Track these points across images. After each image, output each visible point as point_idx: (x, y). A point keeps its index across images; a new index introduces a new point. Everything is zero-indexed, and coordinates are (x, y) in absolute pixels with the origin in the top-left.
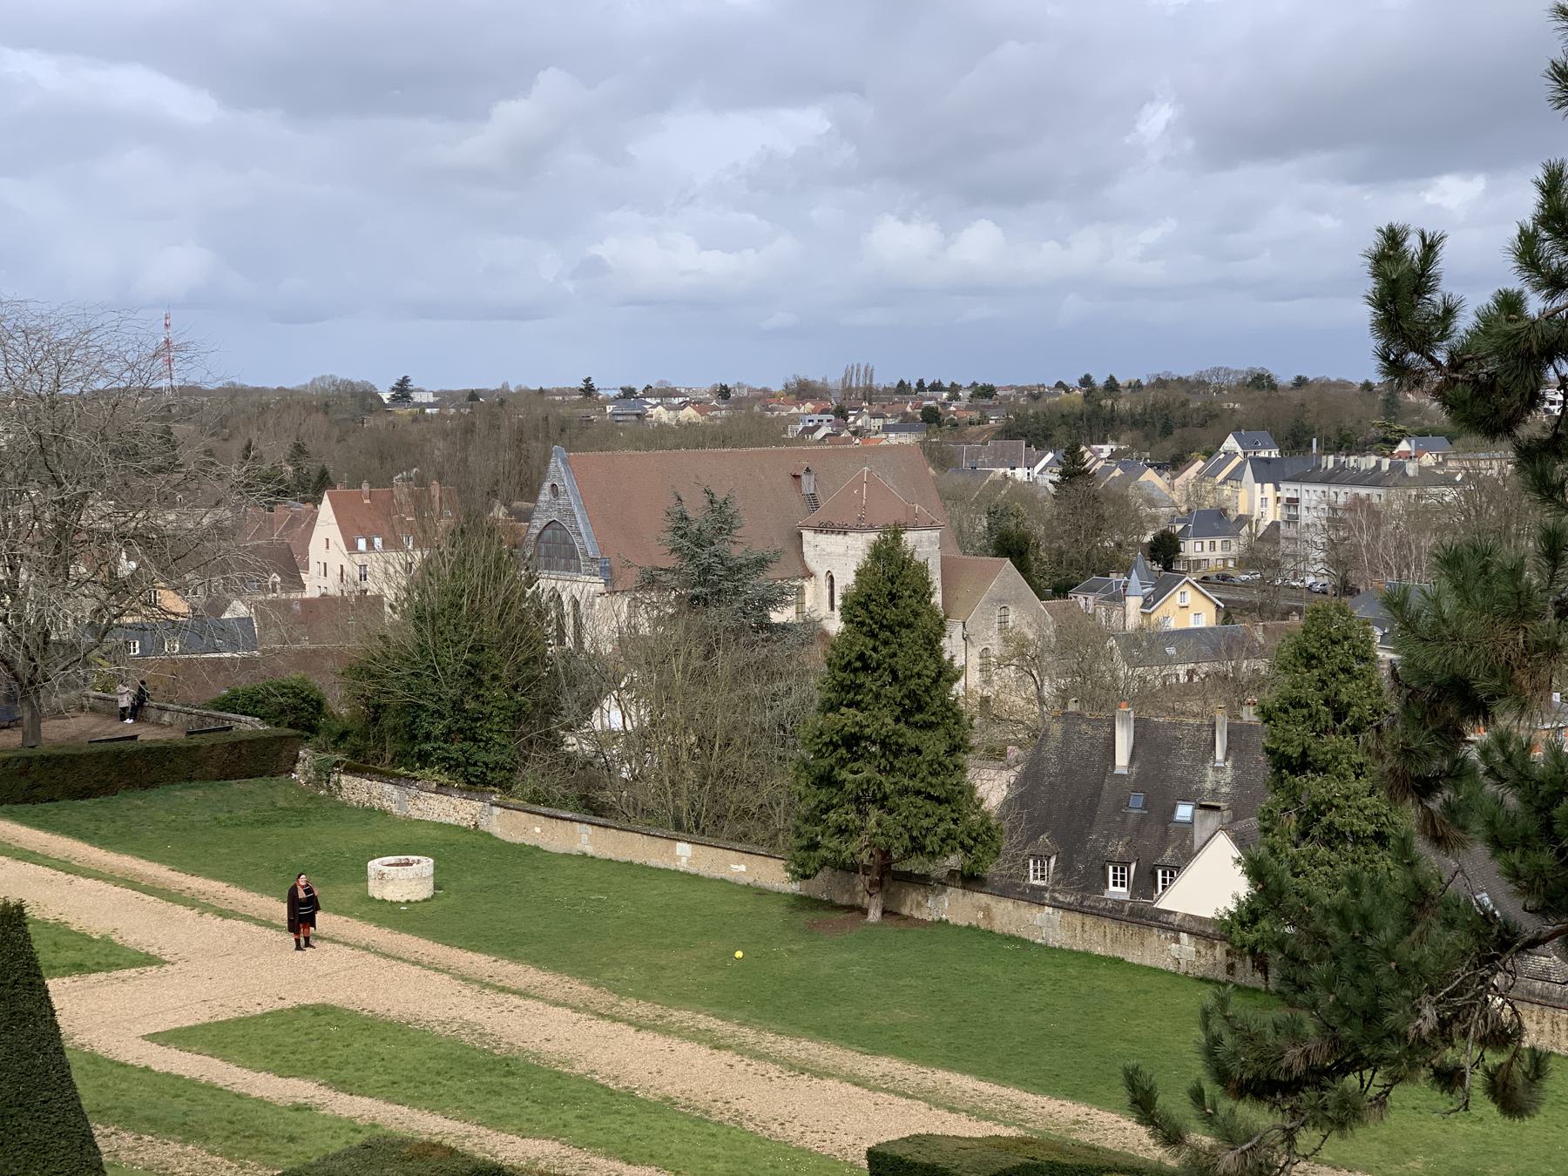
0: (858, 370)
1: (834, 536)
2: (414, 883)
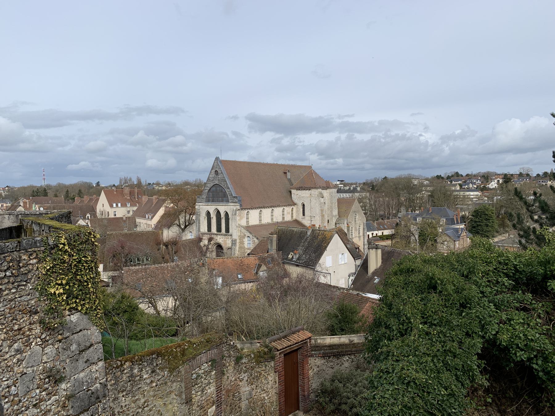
1: (304, 191)
2: (184, 405)
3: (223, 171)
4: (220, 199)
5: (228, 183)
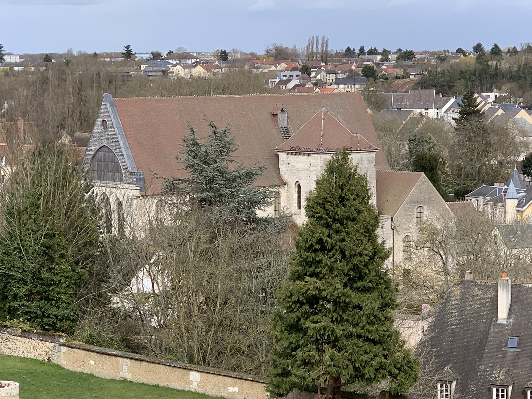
0: (318, 40)
1: (301, 157)
3: (114, 123)
4: (110, 174)
5: (122, 146)
